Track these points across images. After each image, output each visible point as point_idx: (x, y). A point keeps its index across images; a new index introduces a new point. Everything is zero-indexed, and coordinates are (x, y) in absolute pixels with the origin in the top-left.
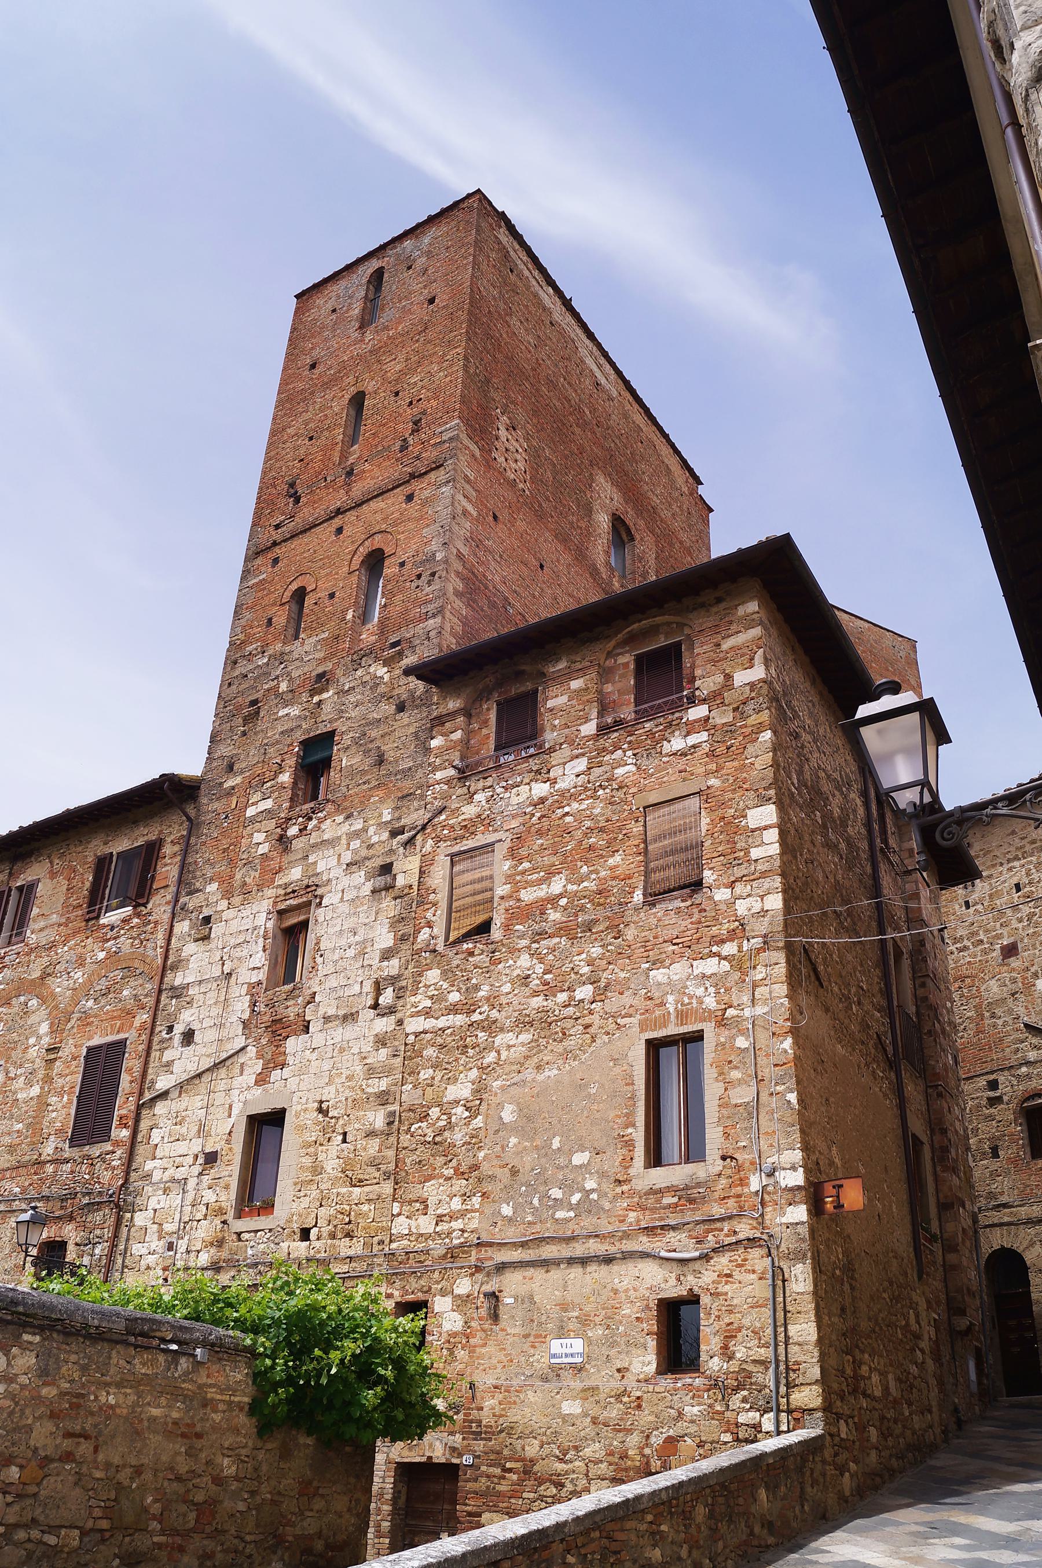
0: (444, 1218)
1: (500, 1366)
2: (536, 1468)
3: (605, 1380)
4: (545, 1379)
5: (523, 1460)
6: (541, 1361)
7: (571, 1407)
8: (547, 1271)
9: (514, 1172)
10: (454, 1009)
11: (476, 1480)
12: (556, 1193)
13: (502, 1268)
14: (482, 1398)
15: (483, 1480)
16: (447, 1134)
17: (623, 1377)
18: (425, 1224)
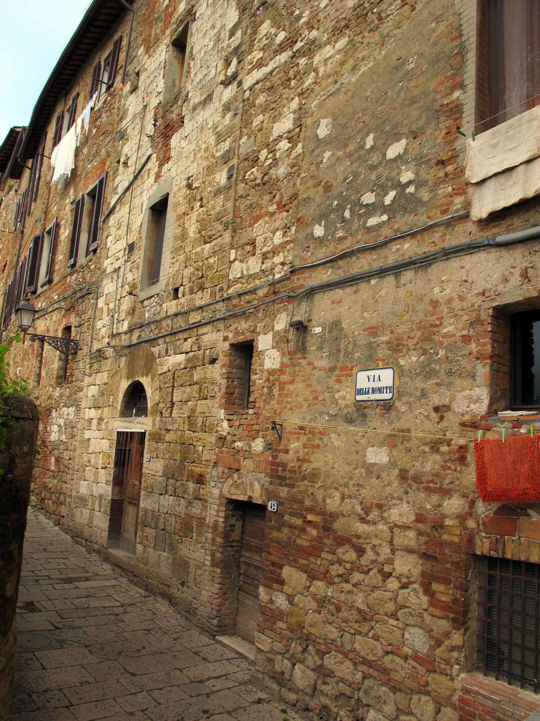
0: (268, 256)
1: (305, 405)
2: (337, 525)
3: (418, 421)
4: (350, 421)
5: (322, 513)
6: (345, 396)
7: (378, 456)
8: (356, 292)
9: (327, 188)
10: (281, 48)
11: (279, 529)
12: (369, 198)
13: (311, 293)
14: (289, 440)
15: (286, 530)
16: (272, 171)
17: (442, 418)
18: (254, 265)
